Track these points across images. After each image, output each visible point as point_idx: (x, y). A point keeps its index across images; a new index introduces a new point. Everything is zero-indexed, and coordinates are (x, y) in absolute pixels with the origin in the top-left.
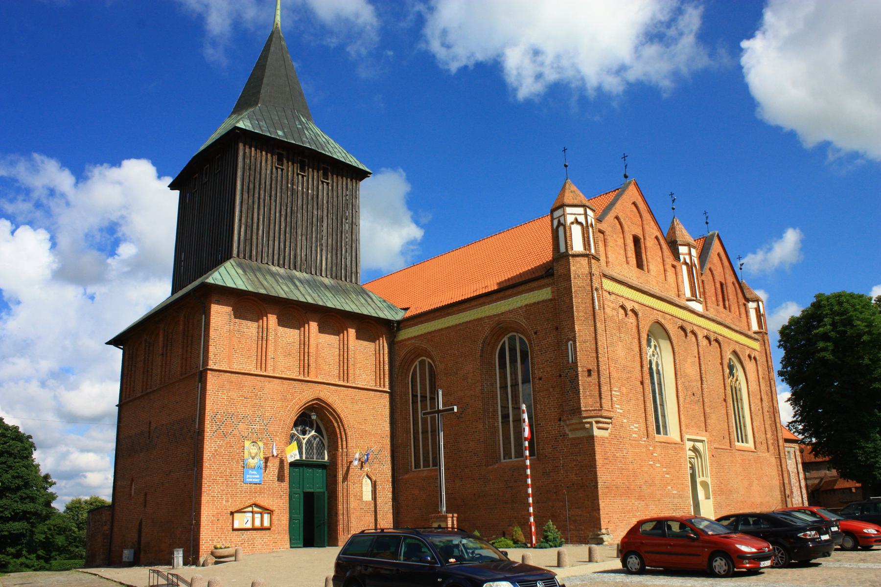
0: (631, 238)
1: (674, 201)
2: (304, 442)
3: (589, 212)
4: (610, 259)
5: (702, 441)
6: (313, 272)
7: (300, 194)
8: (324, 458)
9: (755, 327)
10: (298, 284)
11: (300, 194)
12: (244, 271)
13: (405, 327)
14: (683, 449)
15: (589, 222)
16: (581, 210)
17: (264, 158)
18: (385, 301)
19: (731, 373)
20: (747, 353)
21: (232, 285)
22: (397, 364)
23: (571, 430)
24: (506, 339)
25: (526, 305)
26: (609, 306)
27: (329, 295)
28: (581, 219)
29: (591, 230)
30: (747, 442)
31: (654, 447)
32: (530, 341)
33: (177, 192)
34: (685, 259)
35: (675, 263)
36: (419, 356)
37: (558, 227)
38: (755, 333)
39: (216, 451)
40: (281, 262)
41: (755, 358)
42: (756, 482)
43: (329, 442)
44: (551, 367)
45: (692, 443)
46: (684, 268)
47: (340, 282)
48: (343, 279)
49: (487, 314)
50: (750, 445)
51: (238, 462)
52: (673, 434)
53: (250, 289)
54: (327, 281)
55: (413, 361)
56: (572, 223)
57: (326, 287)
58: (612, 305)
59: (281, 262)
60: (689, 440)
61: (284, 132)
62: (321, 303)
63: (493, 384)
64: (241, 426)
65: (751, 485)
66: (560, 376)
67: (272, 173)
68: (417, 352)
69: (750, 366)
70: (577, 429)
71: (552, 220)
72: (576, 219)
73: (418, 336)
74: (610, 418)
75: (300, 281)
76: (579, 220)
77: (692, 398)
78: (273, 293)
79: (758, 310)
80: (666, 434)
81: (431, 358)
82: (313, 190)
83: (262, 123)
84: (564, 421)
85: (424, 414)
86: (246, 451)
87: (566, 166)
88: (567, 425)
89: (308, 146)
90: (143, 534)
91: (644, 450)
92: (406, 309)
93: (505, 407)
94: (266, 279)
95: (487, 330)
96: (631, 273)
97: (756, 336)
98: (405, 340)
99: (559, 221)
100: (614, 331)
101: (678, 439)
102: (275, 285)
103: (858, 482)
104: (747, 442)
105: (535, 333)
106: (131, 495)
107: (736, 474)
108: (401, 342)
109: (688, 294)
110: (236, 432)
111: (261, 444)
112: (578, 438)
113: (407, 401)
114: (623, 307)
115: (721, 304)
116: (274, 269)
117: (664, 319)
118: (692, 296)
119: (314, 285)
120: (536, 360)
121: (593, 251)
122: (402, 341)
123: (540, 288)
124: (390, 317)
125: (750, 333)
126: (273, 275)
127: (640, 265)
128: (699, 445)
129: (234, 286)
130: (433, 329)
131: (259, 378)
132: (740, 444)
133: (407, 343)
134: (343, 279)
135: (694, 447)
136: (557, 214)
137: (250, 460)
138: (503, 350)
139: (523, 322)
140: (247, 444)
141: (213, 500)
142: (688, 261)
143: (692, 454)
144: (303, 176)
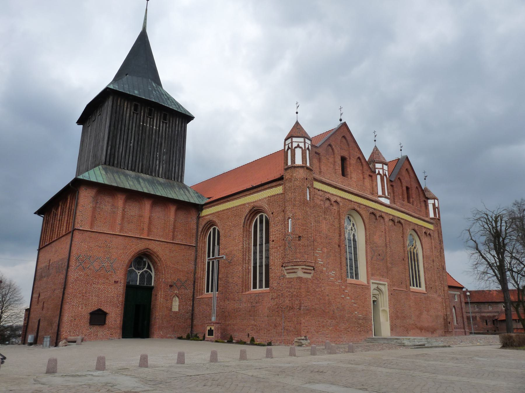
0: (340, 157)
1: (375, 136)
2: (139, 274)
3: (307, 141)
4: (322, 170)
5: (384, 285)
6: (153, 175)
9: (432, 215)
11: (148, 129)
12: (106, 173)
15: (307, 147)
16: (302, 140)
17: (126, 107)
18: (197, 193)
20: (424, 231)
22: (200, 229)
23: (288, 273)
24: (258, 217)
25: (269, 197)
26: (318, 199)
28: (302, 145)
29: (307, 152)
30: (420, 287)
31: (346, 286)
33: (81, 126)
34: (379, 171)
35: (371, 174)
36: (213, 225)
37: (288, 150)
38: (431, 219)
39: (77, 278)
40: (133, 168)
41: (429, 234)
42: (425, 313)
45: (376, 286)
46: (379, 177)
47: (170, 181)
48: (173, 179)
49: (248, 201)
50: (423, 289)
52: (363, 278)
53: (106, 182)
54: (161, 180)
55: (209, 228)
56: (296, 147)
58: (320, 198)
59: (133, 168)
60: (373, 283)
61: (139, 92)
62: (152, 193)
63: (249, 244)
65: (421, 314)
68: (211, 224)
69: (425, 239)
71: (285, 145)
72: (298, 145)
73: (212, 214)
76: (300, 146)
77: (378, 257)
79: (434, 205)
82: (156, 127)
84: (284, 267)
85: (209, 260)
88: (286, 270)
92: (209, 198)
93: (255, 259)
94: (120, 178)
95: (247, 211)
96: (338, 181)
97: (432, 221)
98: (205, 216)
100: (321, 214)
101: (365, 282)
104: (420, 287)
105: (272, 213)
107: (410, 306)
108: (203, 217)
109: (380, 193)
110: (91, 267)
112: (291, 278)
114: (328, 199)
118: (383, 194)
119: (151, 183)
121: (308, 165)
123: (276, 186)
124: (197, 202)
127: (344, 174)
128: (381, 287)
132: (415, 288)
134: (173, 179)
136: (289, 141)
139: (266, 207)
141: (73, 307)
142: (381, 172)
143: (376, 292)
144: (150, 118)
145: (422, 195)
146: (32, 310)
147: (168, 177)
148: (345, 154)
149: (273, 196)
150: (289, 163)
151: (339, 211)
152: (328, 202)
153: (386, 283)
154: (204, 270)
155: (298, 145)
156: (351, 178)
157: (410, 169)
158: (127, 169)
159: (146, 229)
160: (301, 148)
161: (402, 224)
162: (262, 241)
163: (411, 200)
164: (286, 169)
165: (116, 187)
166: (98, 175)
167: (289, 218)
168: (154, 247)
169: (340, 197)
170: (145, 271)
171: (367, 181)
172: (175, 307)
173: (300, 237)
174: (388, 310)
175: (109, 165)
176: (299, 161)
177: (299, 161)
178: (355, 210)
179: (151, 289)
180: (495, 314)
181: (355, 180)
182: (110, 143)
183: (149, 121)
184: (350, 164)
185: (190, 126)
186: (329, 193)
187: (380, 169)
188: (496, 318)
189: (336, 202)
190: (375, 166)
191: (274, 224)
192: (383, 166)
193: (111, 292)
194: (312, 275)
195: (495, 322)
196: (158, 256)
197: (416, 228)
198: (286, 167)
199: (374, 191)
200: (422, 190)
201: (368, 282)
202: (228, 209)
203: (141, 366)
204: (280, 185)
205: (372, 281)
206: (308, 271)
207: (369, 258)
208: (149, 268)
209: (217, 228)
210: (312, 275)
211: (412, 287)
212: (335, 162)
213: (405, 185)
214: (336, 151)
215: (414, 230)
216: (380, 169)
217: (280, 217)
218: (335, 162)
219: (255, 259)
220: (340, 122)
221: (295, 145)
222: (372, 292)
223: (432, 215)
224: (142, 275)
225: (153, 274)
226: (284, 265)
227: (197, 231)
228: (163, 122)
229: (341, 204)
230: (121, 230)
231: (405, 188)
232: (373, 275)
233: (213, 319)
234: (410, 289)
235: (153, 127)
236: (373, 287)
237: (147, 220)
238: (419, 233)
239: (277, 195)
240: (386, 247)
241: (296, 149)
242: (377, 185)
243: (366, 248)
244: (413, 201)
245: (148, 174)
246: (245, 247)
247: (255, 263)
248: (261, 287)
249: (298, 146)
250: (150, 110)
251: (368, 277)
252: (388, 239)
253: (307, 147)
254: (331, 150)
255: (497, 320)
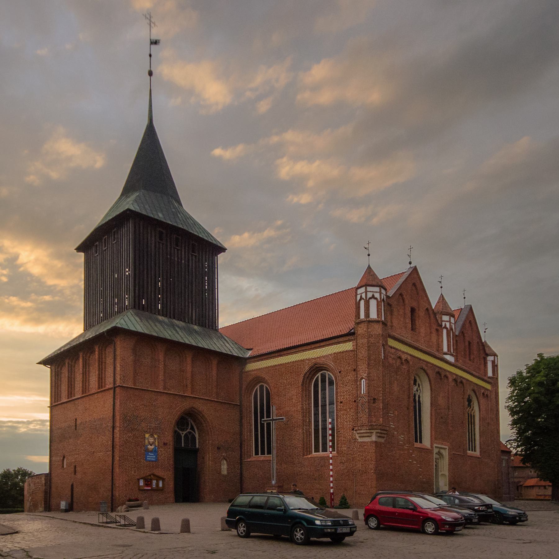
2: (183, 436)
4: (394, 324)
5: (445, 449)
7: (176, 263)
8: (196, 446)
9: (490, 374)
10: (178, 329)
11: (176, 263)
12: (140, 319)
13: (250, 363)
14: (432, 453)
16: (377, 289)
19: (469, 405)
20: (483, 391)
21: (133, 329)
22: (244, 387)
23: (360, 437)
26: (391, 357)
27: (200, 339)
28: (377, 295)
32: (336, 379)
35: (438, 328)
37: (360, 300)
38: (489, 378)
39: (127, 440)
43: (199, 436)
44: (349, 395)
46: (445, 331)
49: (307, 357)
50: (477, 453)
51: (141, 448)
52: (426, 442)
53: (146, 332)
55: (256, 384)
56: (370, 298)
57: (196, 332)
60: (436, 447)
62: (194, 344)
63: (309, 404)
64: (143, 425)
66: (355, 401)
67: (155, 246)
69: (482, 401)
70: (55, 399)
72: (373, 295)
74: (386, 431)
75: (178, 327)
78: (162, 336)
80: (421, 442)
81: (268, 384)
82: (185, 261)
83: (147, 207)
84: (356, 430)
86: (146, 441)
87: (369, 255)
89: (181, 226)
90: (74, 492)
91: (406, 452)
93: (316, 421)
94: (156, 326)
95: (307, 368)
97: (490, 380)
99: (361, 296)
102: (162, 329)
103: (550, 482)
104: (475, 451)
105: (340, 372)
106: (63, 467)
108: (247, 372)
109: (445, 349)
111: (156, 436)
112: (364, 442)
113: (251, 411)
114: (400, 358)
115: (467, 356)
116: (160, 318)
117: (427, 366)
120: (339, 390)
122: (248, 371)
125: (486, 378)
126: (160, 322)
128: (442, 451)
129: (136, 330)
130: (270, 365)
131: (153, 393)
133: (253, 373)
135: (439, 452)
137: (149, 447)
138: (317, 380)
139: (332, 365)
140: (147, 436)
142: (448, 326)
143: (438, 456)
144: (178, 250)
145: (482, 352)
146: (53, 475)
147: (202, 324)
148: (414, 304)
149: (340, 352)
150: (362, 316)
151: (408, 371)
152: (399, 360)
153: (447, 447)
154: (251, 431)
155: (373, 295)
156: (419, 333)
157: (473, 321)
158: (159, 314)
159: (189, 386)
160: (376, 299)
161: (463, 384)
162: (325, 401)
163: (472, 357)
164: (358, 324)
165: (157, 337)
166: (130, 321)
167: (362, 378)
168: (200, 406)
169: (411, 355)
170: (188, 432)
171: (434, 335)
172: (224, 471)
173: (374, 399)
174: (447, 474)
175: (139, 309)
176: (373, 315)
177: (373, 315)
178: (425, 368)
179: (195, 452)
180: (521, 480)
181: (423, 335)
182: (137, 282)
183: (176, 253)
184: (419, 316)
185: (221, 258)
186: (400, 351)
187: (447, 321)
188: (521, 484)
189: (406, 360)
190: (441, 318)
191: (343, 384)
192: (450, 319)
193: (162, 455)
194: (385, 439)
195: (519, 487)
196: (203, 416)
197: (476, 388)
198: (358, 321)
199: (439, 347)
200: (482, 343)
201: (432, 447)
202: (281, 364)
203: (182, 531)
204: (349, 341)
205: (435, 445)
206: (383, 435)
207: (433, 422)
208: (192, 428)
209: (265, 385)
210: (385, 439)
211: (468, 452)
212: (405, 314)
213: (467, 339)
214: (407, 302)
215: (474, 391)
216: (447, 321)
217: (351, 377)
218: (405, 314)
219: (316, 421)
220: (409, 266)
221: (370, 295)
222: (435, 456)
223: (490, 374)
224: (186, 435)
225: (197, 436)
226: (356, 428)
227: (241, 388)
228: (192, 255)
229: (411, 363)
230: (165, 388)
231: (467, 344)
232: (436, 439)
233: (273, 482)
234: (467, 453)
235: (181, 261)
236: (436, 451)
237: (189, 375)
238: (477, 394)
239: (346, 351)
240: (449, 409)
241: (371, 300)
242: (442, 341)
243: (431, 410)
244: (474, 359)
245: (181, 321)
246: (304, 407)
247: (317, 426)
248: (325, 450)
249: (373, 297)
250: (161, 233)
251: (431, 441)
252: (450, 401)
253: (382, 298)
254: (401, 300)
255: (521, 485)
